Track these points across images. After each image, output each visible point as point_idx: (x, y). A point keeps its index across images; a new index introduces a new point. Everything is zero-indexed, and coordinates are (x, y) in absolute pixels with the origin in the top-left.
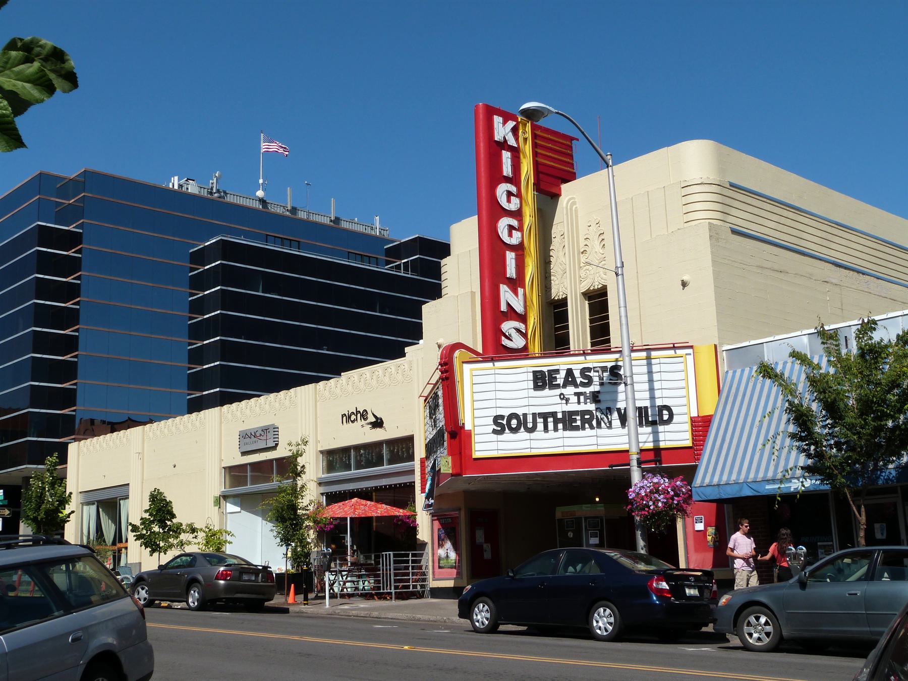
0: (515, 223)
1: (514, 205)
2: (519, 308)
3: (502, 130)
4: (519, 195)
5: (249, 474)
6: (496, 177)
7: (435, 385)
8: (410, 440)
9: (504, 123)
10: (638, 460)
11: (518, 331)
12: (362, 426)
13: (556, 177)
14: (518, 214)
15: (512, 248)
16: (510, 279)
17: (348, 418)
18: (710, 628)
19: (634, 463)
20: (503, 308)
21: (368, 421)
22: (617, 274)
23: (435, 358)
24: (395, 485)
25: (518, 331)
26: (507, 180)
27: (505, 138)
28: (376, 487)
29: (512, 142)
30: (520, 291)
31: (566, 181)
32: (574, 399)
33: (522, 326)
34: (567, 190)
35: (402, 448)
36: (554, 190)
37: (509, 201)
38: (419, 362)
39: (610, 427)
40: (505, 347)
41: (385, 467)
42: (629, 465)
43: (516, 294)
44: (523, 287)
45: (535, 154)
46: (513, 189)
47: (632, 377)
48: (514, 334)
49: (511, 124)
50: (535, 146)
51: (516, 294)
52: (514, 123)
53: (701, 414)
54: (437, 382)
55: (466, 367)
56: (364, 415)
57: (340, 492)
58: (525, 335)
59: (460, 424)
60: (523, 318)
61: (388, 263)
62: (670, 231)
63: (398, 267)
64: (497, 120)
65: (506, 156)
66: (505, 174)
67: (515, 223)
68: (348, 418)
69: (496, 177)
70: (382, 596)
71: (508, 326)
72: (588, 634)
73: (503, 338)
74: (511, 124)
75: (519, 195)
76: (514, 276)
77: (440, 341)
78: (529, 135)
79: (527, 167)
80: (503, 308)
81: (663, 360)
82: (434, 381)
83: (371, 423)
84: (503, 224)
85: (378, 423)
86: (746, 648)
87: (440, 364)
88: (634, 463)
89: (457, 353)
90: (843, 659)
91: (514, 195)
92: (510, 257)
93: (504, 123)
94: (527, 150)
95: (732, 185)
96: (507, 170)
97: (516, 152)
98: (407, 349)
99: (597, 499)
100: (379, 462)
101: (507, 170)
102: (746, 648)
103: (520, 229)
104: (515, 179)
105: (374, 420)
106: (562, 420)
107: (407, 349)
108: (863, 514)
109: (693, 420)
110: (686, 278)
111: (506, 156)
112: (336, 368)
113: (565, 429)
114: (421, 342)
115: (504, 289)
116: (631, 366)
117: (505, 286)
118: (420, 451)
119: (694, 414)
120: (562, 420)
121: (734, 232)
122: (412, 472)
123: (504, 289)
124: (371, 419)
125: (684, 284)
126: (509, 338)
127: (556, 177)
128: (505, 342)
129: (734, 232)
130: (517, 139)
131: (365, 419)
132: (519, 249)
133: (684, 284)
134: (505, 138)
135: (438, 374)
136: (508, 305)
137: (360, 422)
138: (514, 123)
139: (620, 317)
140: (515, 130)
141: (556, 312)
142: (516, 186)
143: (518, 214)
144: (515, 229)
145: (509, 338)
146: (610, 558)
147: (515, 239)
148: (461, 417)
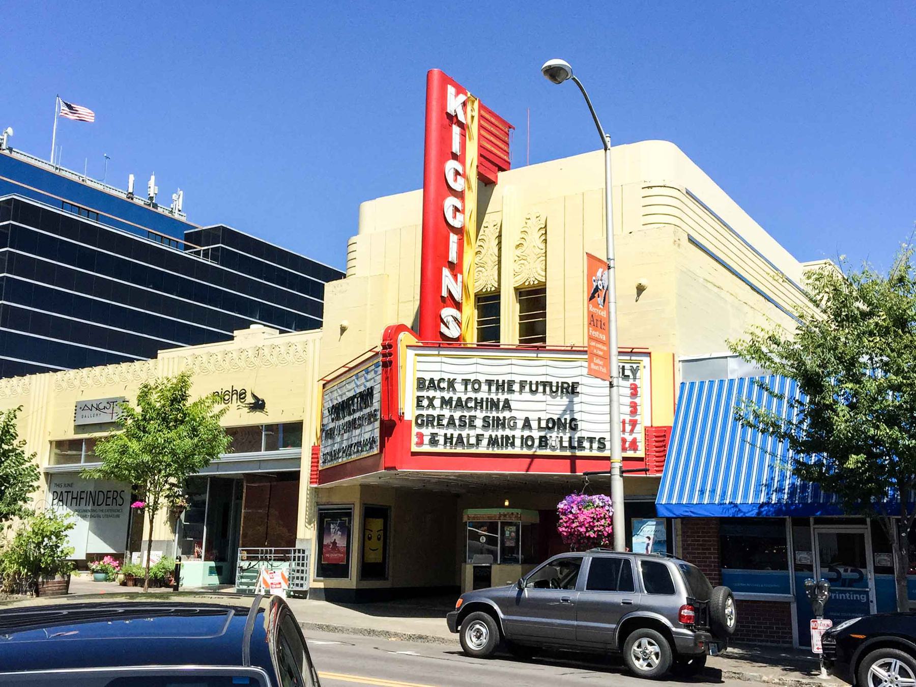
2: (457, 297)
3: (454, 103)
5: (83, 453)
9: (458, 94)
11: (455, 319)
13: (496, 165)
19: (616, 472)
25: (455, 319)
26: (455, 157)
29: (461, 118)
30: (459, 277)
32: (485, 387)
34: (502, 177)
35: (291, 433)
36: (491, 177)
37: (456, 180)
39: (539, 420)
40: (442, 334)
41: (263, 452)
42: (610, 472)
44: (461, 273)
48: (452, 325)
49: (462, 98)
56: (242, 395)
58: (459, 324)
64: (451, 90)
65: (456, 130)
66: (454, 151)
71: (447, 313)
73: (442, 325)
74: (462, 98)
80: (444, 293)
81: (514, 361)
84: (450, 202)
85: (258, 405)
88: (616, 472)
92: (453, 238)
93: (458, 94)
95: (688, 192)
99: (507, 503)
100: (570, 584)
109: (646, 428)
110: (345, 324)
115: (446, 272)
118: (310, 436)
121: (691, 240)
123: (446, 272)
124: (250, 400)
127: (496, 165)
128: (443, 329)
129: (691, 240)
130: (465, 113)
141: (488, 304)
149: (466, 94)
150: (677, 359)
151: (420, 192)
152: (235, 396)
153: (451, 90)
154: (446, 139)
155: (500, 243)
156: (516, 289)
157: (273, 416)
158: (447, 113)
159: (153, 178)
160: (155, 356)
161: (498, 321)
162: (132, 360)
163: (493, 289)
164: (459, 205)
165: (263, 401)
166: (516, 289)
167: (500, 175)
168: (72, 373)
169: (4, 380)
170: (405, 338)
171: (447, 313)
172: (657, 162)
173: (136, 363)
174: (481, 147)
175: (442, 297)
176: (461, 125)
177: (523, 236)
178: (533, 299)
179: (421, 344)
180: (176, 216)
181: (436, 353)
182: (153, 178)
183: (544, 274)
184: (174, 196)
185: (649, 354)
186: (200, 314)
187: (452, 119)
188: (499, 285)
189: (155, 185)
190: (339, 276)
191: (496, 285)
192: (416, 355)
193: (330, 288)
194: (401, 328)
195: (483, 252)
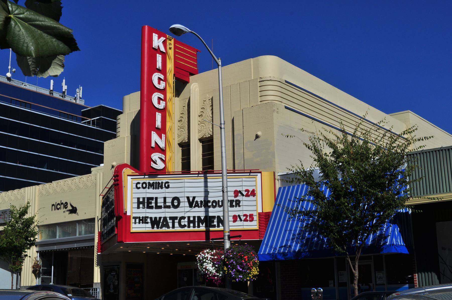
1: (162, 86)
2: (162, 145)
3: (157, 42)
4: (165, 80)
6: (153, 69)
7: (110, 188)
8: (93, 220)
9: (159, 38)
12: (64, 212)
14: (163, 91)
16: (158, 129)
17: (56, 207)
19: (227, 237)
20: (153, 145)
21: (68, 209)
22: (221, 128)
23: (111, 173)
24: (82, 247)
25: (161, 159)
26: (158, 71)
27: (158, 46)
28: (71, 248)
29: (162, 49)
31: (192, 74)
33: (163, 157)
36: (185, 79)
37: (159, 83)
38: (100, 176)
39: (165, 198)
43: (161, 137)
44: (165, 133)
45: (175, 58)
46: (162, 77)
47: (227, 187)
48: (159, 161)
49: (163, 39)
50: (175, 53)
51: (161, 137)
52: (164, 39)
53: (264, 211)
55: (129, 178)
57: (48, 251)
58: (164, 161)
59: (124, 212)
60: (163, 151)
61: (83, 120)
62: (251, 106)
63: (89, 123)
64: (155, 36)
65: (159, 58)
67: (162, 96)
68: (56, 207)
69: (153, 69)
71: (155, 156)
73: (152, 163)
74: (163, 39)
78: (172, 46)
79: (170, 65)
80: (153, 145)
82: (109, 186)
83: (69, 210)
84: (155, 97)
85: (74, 210)
87: (114, 176)
89: (124, 170)
91: (162, 80)
92: (159, 116)
93: (159, 38)
94: (171, 53)
95: (286, 82)
96: (159, 65)
97: (164, 55)
98: (92, 169)
101: (159, 65)
103: (165, 100)
104: (163, 71)
105: (71, 208)
106: (142, 220)
107: (92, 169)
108: (357, 268)
109: (259, 213)
110: (259, 133)
111: (159, 58)
112: (49, 178)
113: (143, 223)
114: (102, 165)
116: (227, 182)
117: (154, 132)
120: (142, 220)
121: (286, 108)
122: (93, 240)
124: (69, 208)
125: (257, 137)
128: (153, 165)
129: (286, 108)
131: (66, 208)
132: (164, 111)
133: (257, 137)
134: (158, 46)
136: (156, 143)
137: (63, 210)
138: (164, 39)
139: (222, 153)
140: (164, 43)
142: (163, 74)
143: (163, 91)
144: (162, 100)
149: (165, 37)
150: (277, 174)
152: (62, 205)
153: (155, 36)
154: (153, 61)
155: (212, 109)
157: (80, 216)
158: (154, 48)
159: (64, 81)
160: (90, 172)
161: (212, 154)
162: (38, 184)
163: (209, 136)
165: (76, 208)
167: (191, 78)
168: (47, 185)
169: (4, 193)
170: (127, 171)
171: (155, 156)
172: (271, 65)
173: (40, 186)
175: (153, 147)
176: (161, 53)
177: (202, 110)
180: (78, 102)
182: (64, 81)
183: (212, 130)
184: (77, 90)
185: (260, 172)
186: (41, 162)
187: (158, 50)
188: (213, 134)
189: (66, 85)
191: (211, 133)
193: (107, 144)
194: (125, 166)
195: (204, 115)
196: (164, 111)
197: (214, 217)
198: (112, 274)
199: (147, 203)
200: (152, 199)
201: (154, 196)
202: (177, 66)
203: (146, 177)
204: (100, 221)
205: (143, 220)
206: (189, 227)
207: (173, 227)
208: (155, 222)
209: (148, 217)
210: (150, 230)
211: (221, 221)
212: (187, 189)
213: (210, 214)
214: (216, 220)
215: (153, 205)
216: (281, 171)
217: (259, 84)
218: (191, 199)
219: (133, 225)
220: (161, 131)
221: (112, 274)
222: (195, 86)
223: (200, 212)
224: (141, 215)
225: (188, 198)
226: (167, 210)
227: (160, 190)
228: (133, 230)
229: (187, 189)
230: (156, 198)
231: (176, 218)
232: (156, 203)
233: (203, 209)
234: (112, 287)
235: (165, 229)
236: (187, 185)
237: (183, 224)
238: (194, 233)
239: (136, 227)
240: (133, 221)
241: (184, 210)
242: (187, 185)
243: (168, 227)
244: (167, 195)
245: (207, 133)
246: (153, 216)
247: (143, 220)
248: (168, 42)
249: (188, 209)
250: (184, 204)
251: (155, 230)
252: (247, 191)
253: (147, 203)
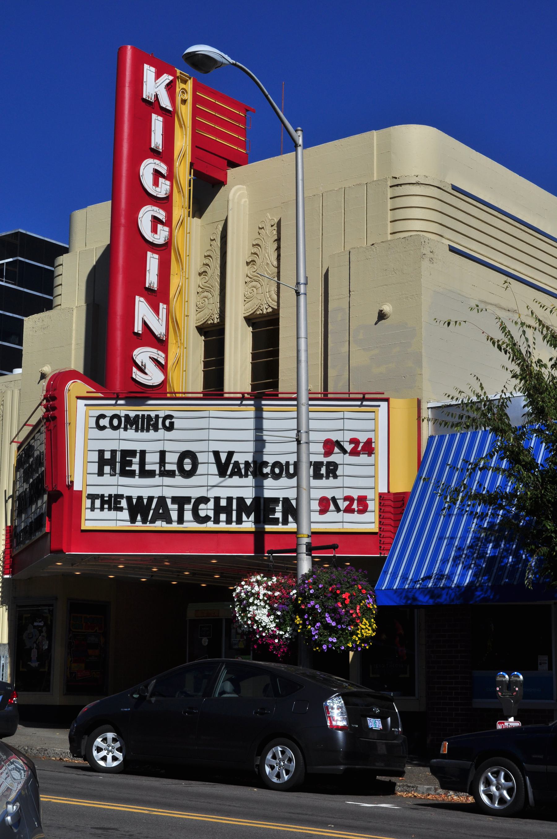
0: (161, 215)
2: (159, 329)
3: (154, 85)
4: (170, 177)
7: (35, 427)
9: (158, 75)
10: (308, 546)
14: (165, 203)
15: (154, 247)
18: (256, 770)
19: (303, 549)
20: (138, 328)
22: (298, 294)
23: (39, 391)
25: (156, 362)
26: (155, 154)
29: (165, 102)
30: (162, 307)
31: (234, 165)
36: (218, 176)
39: (163, 454)
43: (145, 324)
47: (307, 432)
48: (151, 367)
49: (166, 78)
50: (196, 112)
52: (171, 78)
53: (393, 490)
54: (40, 422)
55: (81, 403)
58: (163, 367)
62: (370, 243)
64: (149, 72)
65: (157, 123)
70: (353, 511)
71: (143, 355)
72: (262, 782)
73: (134, 369)
74: (166, 78)
75: (170, 177)
76: (155, 287)
77: (47, 369)
78: (189, 97)
79: (183, 142)
80: (138, 328)
81: (347, 415)
82: (34, 421)
84: (146, 215)
86: (478, 808)
87: (45, 398)
90: (151, 778)
91: (163, 176)
92: (153, 262)
93: (158, 75)
94: (185, 112)
95: (454, 188)
96: (157, 139)
97: (169, 117)
101: (157, 139)
102: (478, 808)
104: (166, 155)
109: (381, 495)
110: (387, 308)
111: (157, 123)
114: (17, 371)
117: (142, 299)
119: (383, 489)
121: (452, 249)
125: (382, 316)
126: (142, 370)
128: (137, 375)
129: (452, 249)
132: (165, 250)
133: (382, 316)
135: (41, 412)
136: (145, 324)
138: (171, 78)
139: (298, 351)
140: (170, 87)
143: (165, 203)
144: (161, 222)
145: (142, 370)
146: (89, 709)
147: (160, 237)
148: (69, 472)
149: (173, 73)
151: (110, 202)
153: (149, 72)
154: (142, 130)
156: (196, 327)
158: (145, 101)
164: (161, 215)
166: (196, 327)
167: (232, 173)
170: (75, 388)
171: (143, 355)
172: (420, 148)
174: (195, 136)
175: (137, 334)
176: (163, 112)
177: (255, 250)
178: (266, 329)
179: (100, 395)
181: (113, 402)
187: (154, 106)
190: (66, 251)
192: (86, 405)
194: (72, 375)
196: (165, 250)
197: (276, 501)
198: (35, 624)
199: (122, 463)
200: (132, 453)
201: (137, 447)
202: (198, 144)
203: (120, 402)
204: (10, 501)
205: (111, 502)
206: (217, 521)
207: (181, 520)
208: (138, 508)
209: (121, 496)
210: (127, 525)
211: (291, 510)
212: (214, 435)
213: (268, 494)
214: (279, 508)
215: (135, 467)
216: (433, 399)
217: (390, 193)
218: (223, 457)
219: (87, 514)
220: (158, 297)
221: (35, 624)
222: (239, 192)
223: (243, 488)
224: (106, 492)
225: (216, 454)
226: (167, 480)
227: (152, 434)
228: (86, 525)
229: (214, 435)
230: (143, 453)
231: (187, 500)
232: (142, 463)
233: (250, 480)
234: (34, 654)
235: (160, 525)
236: (215, 423)
237: (202, 514)
238: (227, 536)
239: (93, 519)
240: (87, 503)
241: (206, 483)
242: (215, 423)
243: (169, 521)
244: (168, 446)
245: (264, 303)
246: (135, 493)
247: (111, 502)
248: (180, 86)
249: (217, 480)
250: (208, 467)
251: (139, 525)
252: (355, 441)
253: (122, 463)
